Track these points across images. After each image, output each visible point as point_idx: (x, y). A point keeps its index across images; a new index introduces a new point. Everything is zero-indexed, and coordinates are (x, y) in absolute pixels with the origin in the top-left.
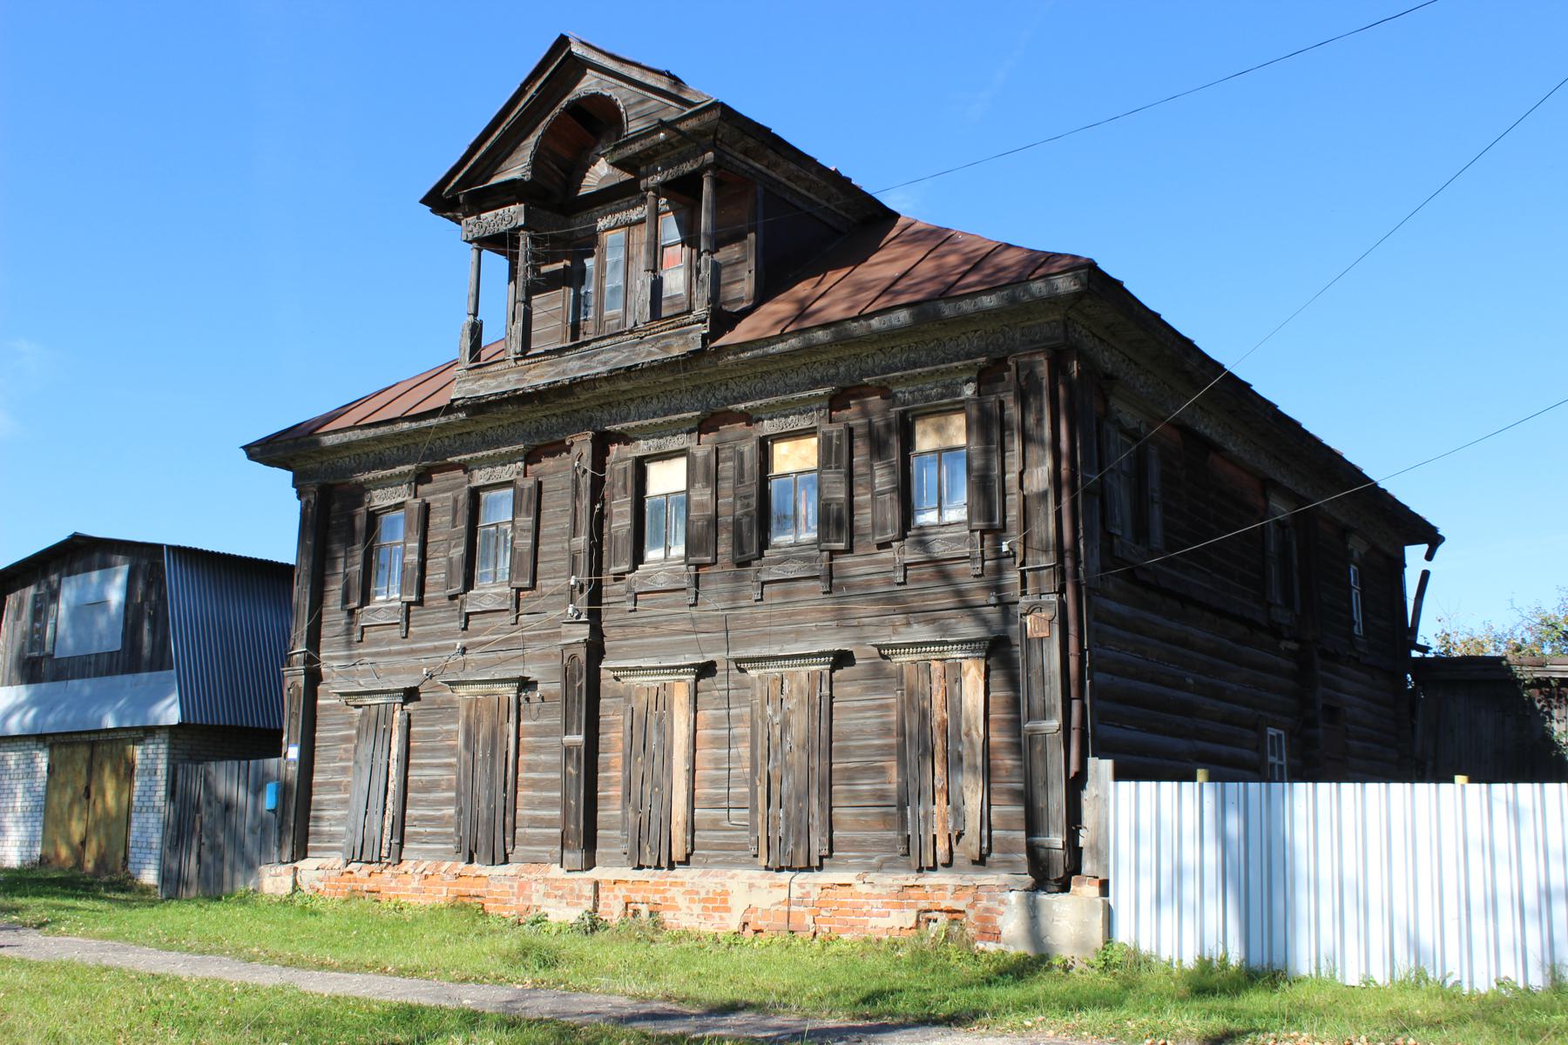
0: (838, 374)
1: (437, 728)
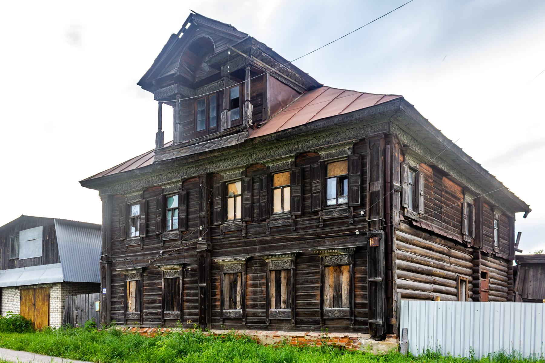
0: (298, 147)
1: (154, 282)
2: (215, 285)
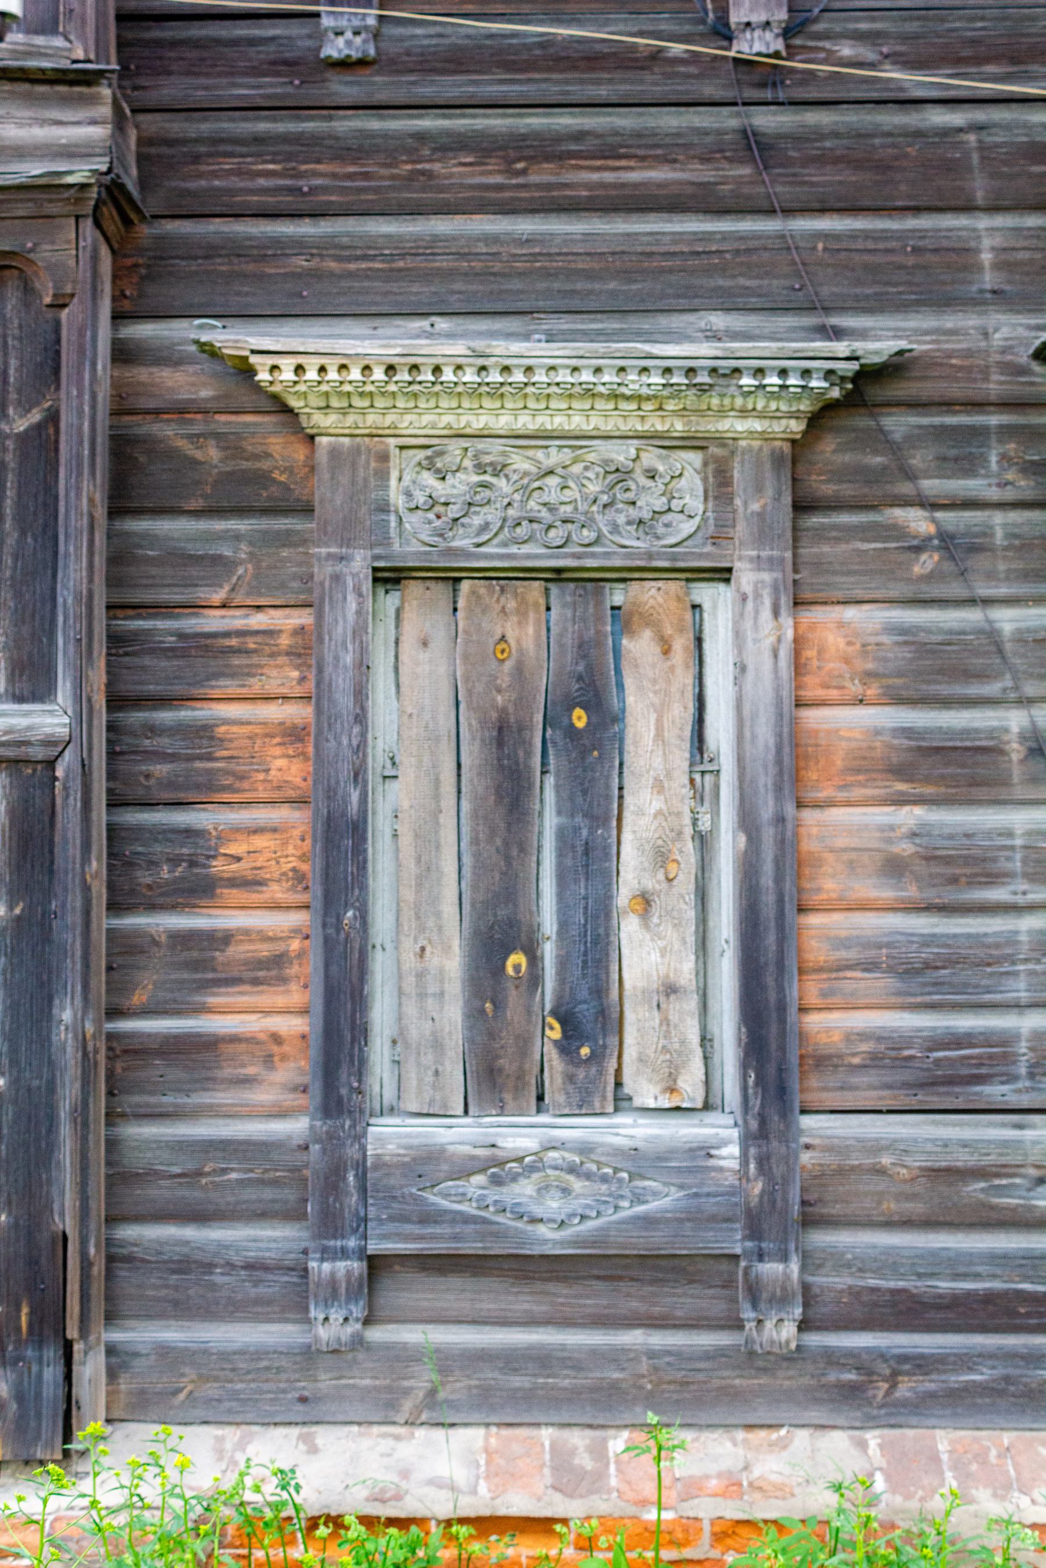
2: (204, 731)
